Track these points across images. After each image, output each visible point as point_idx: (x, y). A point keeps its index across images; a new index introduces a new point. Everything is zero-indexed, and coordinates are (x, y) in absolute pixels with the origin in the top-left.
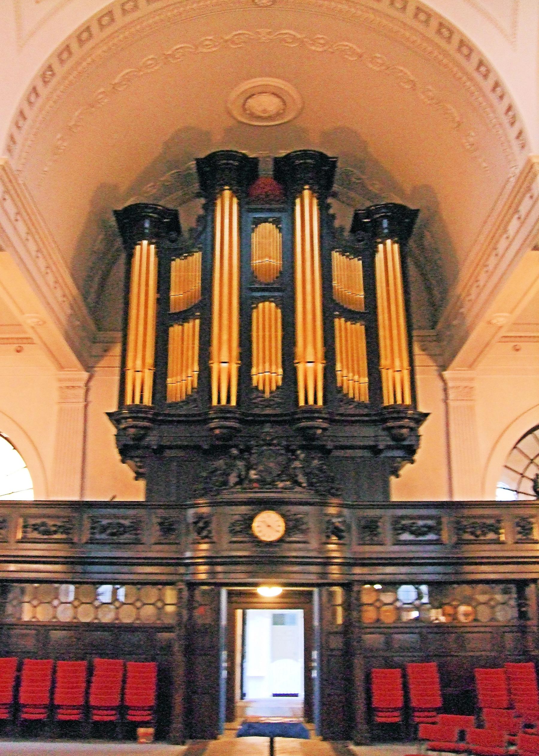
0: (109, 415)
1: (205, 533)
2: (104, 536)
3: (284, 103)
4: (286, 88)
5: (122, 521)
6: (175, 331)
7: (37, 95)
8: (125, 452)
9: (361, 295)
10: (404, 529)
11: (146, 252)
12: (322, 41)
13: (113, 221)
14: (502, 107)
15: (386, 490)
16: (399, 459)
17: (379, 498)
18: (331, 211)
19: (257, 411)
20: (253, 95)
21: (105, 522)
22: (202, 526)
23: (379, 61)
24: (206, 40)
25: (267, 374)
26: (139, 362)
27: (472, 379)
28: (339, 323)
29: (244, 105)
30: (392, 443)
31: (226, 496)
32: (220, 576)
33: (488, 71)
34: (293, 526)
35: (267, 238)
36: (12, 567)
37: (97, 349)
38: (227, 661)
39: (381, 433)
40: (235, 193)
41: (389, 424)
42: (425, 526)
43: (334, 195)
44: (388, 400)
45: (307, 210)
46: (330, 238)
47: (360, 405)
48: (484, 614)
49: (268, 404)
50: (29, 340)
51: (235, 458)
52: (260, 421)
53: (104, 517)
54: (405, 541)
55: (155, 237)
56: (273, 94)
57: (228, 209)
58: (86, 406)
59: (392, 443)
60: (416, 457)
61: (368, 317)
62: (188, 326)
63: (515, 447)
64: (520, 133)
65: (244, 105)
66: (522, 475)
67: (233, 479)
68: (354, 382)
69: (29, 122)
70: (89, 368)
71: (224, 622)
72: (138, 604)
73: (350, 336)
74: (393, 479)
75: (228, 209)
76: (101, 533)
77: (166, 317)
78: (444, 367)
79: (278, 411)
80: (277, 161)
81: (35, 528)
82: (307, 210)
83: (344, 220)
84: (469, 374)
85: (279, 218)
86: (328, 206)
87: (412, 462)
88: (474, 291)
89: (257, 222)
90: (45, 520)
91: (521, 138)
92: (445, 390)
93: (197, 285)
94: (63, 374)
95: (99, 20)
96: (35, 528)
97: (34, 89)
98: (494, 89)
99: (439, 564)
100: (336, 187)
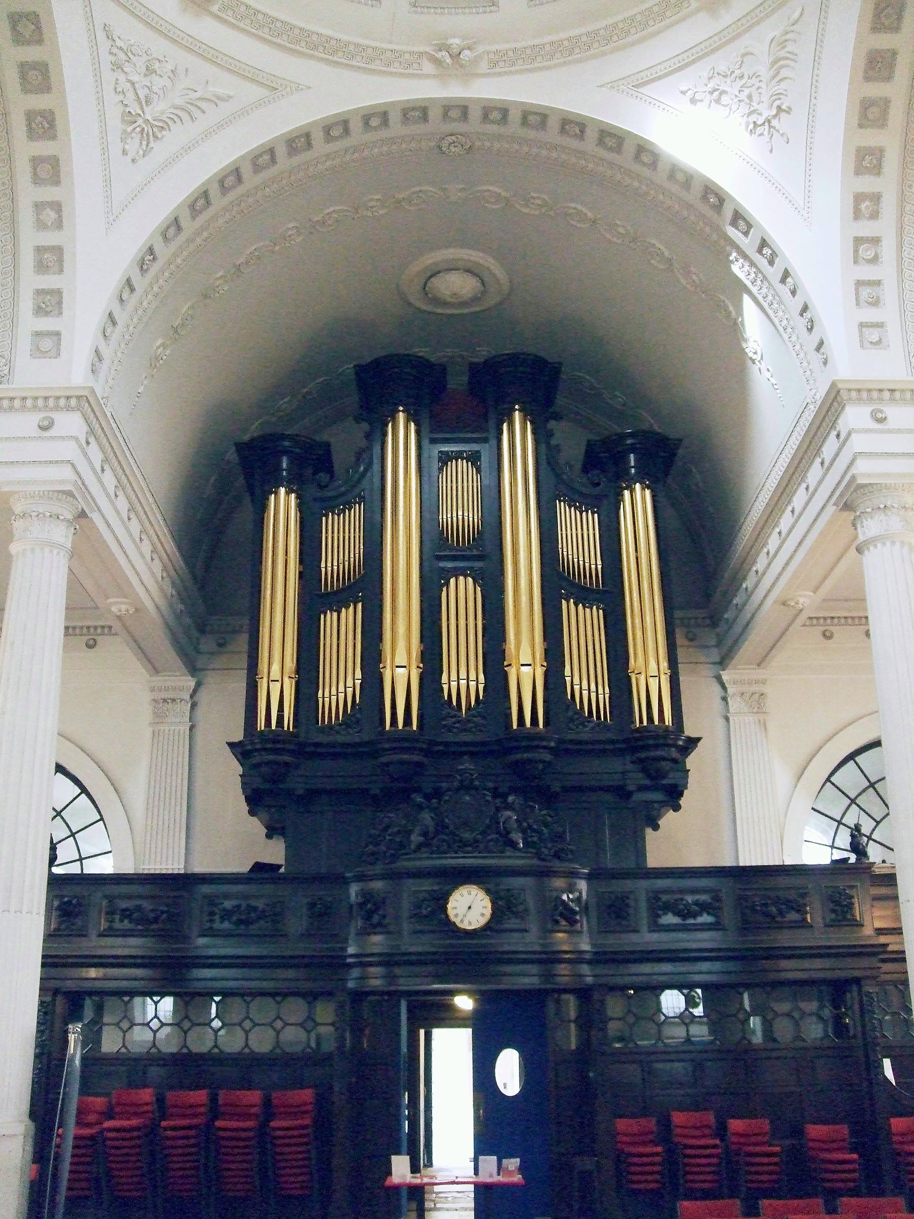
0: (231, 745)
1: (376, 919)
2: (226, 925)
3: (483, 284)
4: (486, 264)
5: (253, 903)
6: (328, 621)
7: (132, 290)
8: (256, 800)
9: (605, 693)
10: (668, 908)
11: (283, 506)
12: (538, 202)
13: (232, 455)
14: (795, 305)
15: (641, 853)
16: (656, 805)
17: (629, 863)
18: (553, 442)
19: (450, 737)
20: (439, 272)
21: (228, 904)
22: (372, 912)
23: (621, 230)
24: (372, 200)
25: (463, 679)
26: (276, 668)
27: (764, 682)
28: (568, 608)
29: (426, 284)
30: (647, 782)
31: (405, 864)
32: (402, 981)
33: (774, 255)
34: (504, 908)
35: (460, 487)
36: (93, 973)
37: (208, 643)
38: (408, 1107)
39: (629, 767)
40: (412, 416)
41: (643, 755)
42: (696, 903)
43: (557, 417)
44: (640, 718)
45: (518, 441)
46: (553, 487)
47: (601, 726)
48: (784, 1030)
49: (464, 725)
50: (108, 630)
51: (420, 807)
52: (453, 752)
53: (227, 896)
54: (669, 925)
55: (296, 484)
56: (468, 271)
57: (402, 439)
58: (191, 728)
59: (647, 782)
60: (683, 802)
61: (608, 595)
62: (347, 614)
63: (828, 780)
64: (821, 344)
65: (426, 284)
66: (840, 823)
67: (416, 838)
68: (588, 686)
69: (120, 327)
70: (193, 669)
71: (404, 1049)
72: (279, 1024)
73: (583, 624)
74: (649, 831)
75: (402, 439)
76: (223, 919)
77: (315, 600)
78: (723, 663)
79: (480, 737)
80: (474, 370)
81: (126, 914)
82: (518, 441)
83: (572, 444)
84: (759, 674)
85: (478, 452)
86: (550, 434)
87: (677, 808)
88: (760, 565)
89: (445, 459)
90: (139, 902)
91: (822, 350)
92: (724, 699)
93: (357, 549)
94: (158, 681)
95: (222, 182)
96: (126, 914)
97: (129, 282)
98: (783, 281)
99: (717, 959)
100: (561, 401)
